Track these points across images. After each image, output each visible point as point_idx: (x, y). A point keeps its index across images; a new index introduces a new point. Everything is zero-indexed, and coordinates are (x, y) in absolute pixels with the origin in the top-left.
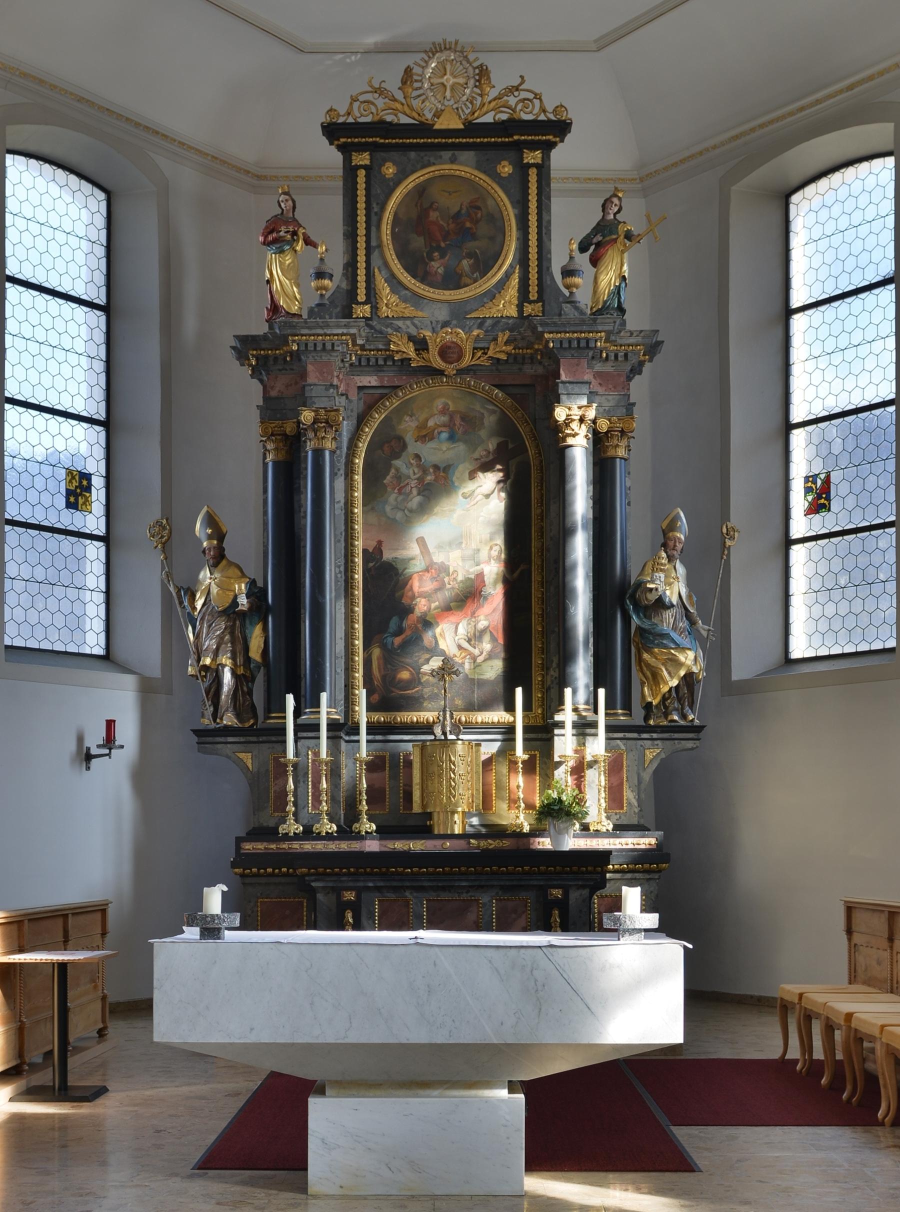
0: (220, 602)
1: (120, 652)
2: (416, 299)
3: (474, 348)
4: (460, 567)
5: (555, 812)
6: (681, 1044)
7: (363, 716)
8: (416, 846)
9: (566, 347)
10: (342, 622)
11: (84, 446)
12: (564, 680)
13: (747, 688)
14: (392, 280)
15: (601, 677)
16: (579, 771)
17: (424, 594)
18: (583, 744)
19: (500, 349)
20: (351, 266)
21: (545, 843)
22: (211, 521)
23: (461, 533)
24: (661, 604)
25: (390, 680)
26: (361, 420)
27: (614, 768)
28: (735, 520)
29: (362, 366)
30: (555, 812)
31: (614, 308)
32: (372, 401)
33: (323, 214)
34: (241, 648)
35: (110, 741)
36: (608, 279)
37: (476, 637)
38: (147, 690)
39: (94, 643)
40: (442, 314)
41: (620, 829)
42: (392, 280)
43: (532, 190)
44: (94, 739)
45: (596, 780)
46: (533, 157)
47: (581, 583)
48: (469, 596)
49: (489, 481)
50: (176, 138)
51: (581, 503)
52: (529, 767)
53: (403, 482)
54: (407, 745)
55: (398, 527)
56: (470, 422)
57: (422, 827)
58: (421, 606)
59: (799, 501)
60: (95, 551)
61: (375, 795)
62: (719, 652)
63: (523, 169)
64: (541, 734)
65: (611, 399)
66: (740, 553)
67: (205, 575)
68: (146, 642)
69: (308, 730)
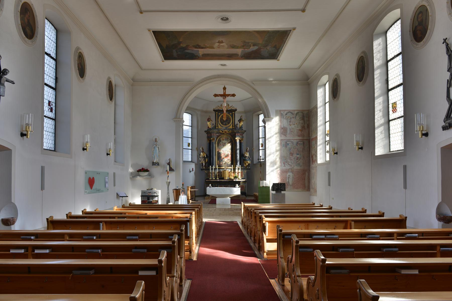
0: (203, 156)
1: (193, 161)
2: (222, 127)
4: (226, 153)
5: (235, 177)
6: (239, 195)
7: (217, 167)
8: (223, 180)
9: (237, 132)
10: (215, 158)
11: (190, 141)
12: (237, 164)
13: (255, 164)
15: (240, 164)
16: (238, 173)
17: (223, 156)
18: (239, 171)
19: (230, 132)
20: (216, 123)
21: (235, 180)
23: (226, 150)
24: (246, 157)
25: (220, 164)
26: (217, 138)
27: (242, 173)
28: (254, 147)
29: (217, 133)
30: (235, 177)
31: (241, 128)
32: (218, 136)
33: (213, 118)
35: (193, 170)
36: (241, 125)
37: (228, 160)
38: (196, 165)
39: (190, 160)
41: (242, 179)
43: (233, 116)
44: (191, 170)
45: (240, 174)
46: (233, 113)
47: (238, 155)
48: (227, 156)
49: (229, 144)
51: (238, 147)
52: (233, 173)
53: (221, 144)
54: (221, 170)
55: (220, 149)
56: (228, 139)
57: (223, 179)
58: (223, 157)
59: (260, 146)
60: (190, 151)
61: (218, 175)
62: (252, 161)
64: (234, 169)
65: (241, 137)
66: (254, 151)
67: (202, 153)
68: (195, 160)
69: (212, 169)
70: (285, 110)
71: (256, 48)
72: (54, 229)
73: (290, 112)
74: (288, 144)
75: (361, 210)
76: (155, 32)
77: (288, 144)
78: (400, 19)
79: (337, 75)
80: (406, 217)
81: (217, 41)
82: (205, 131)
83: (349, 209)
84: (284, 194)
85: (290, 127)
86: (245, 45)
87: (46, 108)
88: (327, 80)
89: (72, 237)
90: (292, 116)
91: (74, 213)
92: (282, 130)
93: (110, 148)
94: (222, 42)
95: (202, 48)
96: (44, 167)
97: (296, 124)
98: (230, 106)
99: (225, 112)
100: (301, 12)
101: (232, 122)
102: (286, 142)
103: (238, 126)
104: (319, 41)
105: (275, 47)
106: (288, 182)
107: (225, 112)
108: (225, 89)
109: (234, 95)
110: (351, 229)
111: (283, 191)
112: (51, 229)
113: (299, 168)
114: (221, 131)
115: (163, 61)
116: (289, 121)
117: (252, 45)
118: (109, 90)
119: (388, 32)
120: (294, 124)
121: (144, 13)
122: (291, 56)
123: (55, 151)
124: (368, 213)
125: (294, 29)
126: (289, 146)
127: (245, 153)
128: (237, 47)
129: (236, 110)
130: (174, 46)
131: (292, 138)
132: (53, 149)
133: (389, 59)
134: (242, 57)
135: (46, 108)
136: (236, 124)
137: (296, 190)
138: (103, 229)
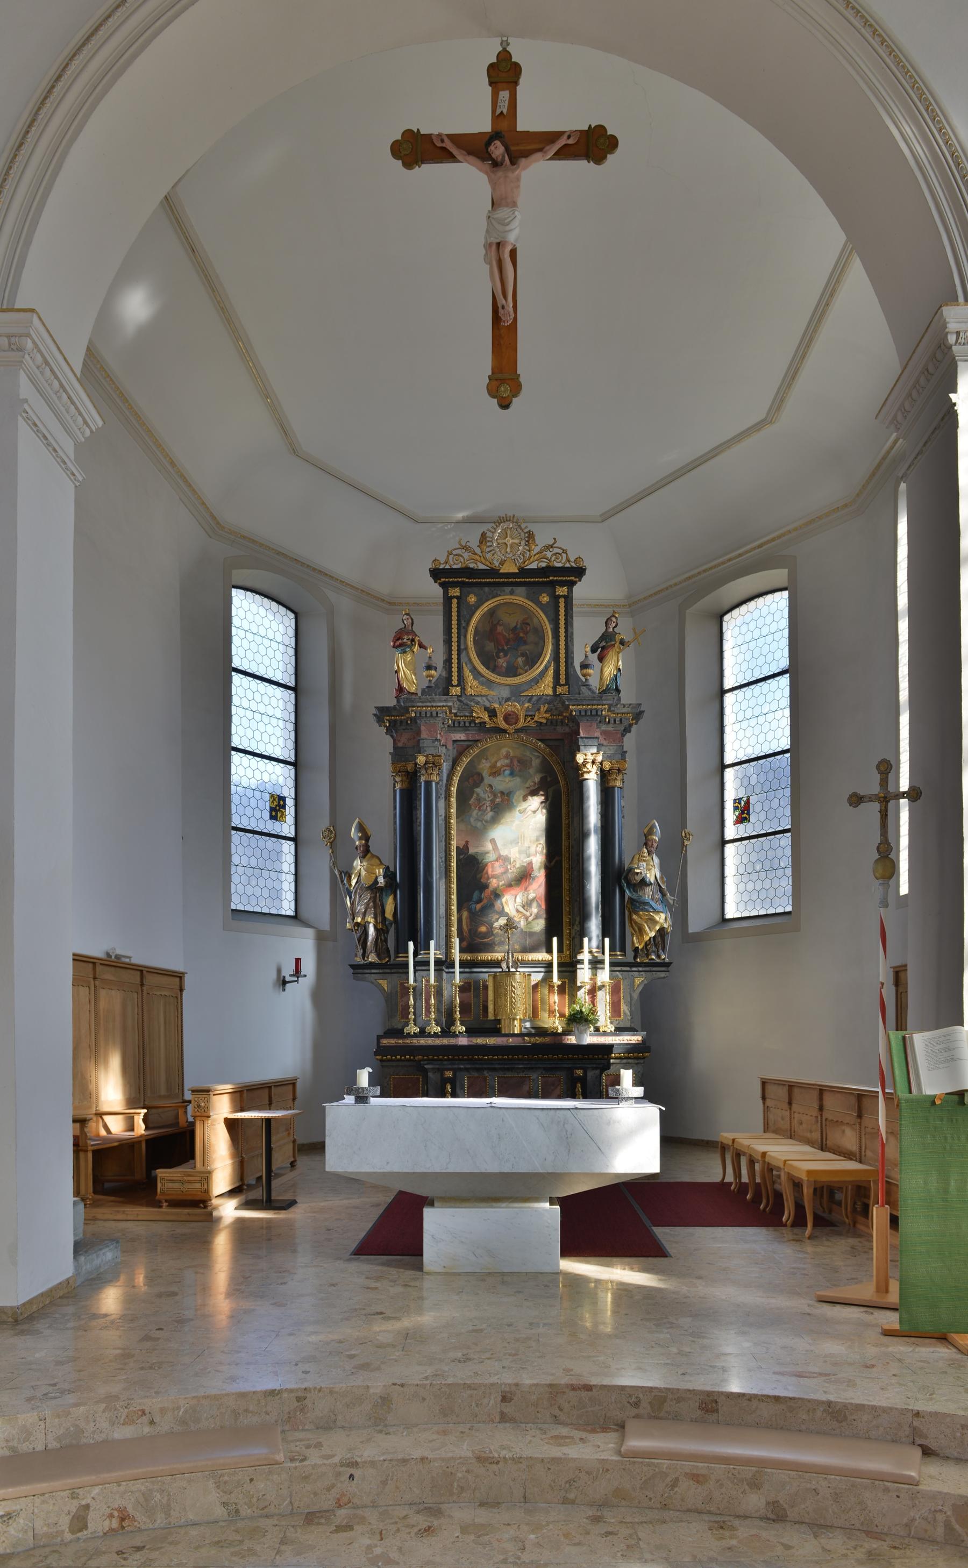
14: (474, 670)
20: (448, 661)
22: (361, 828)
35: (297, 972)
42: (474, 670)
43: (561, 613)
44: (288, 971)
63: (556, 598)
108: (504, 73)
136: (577, 660)
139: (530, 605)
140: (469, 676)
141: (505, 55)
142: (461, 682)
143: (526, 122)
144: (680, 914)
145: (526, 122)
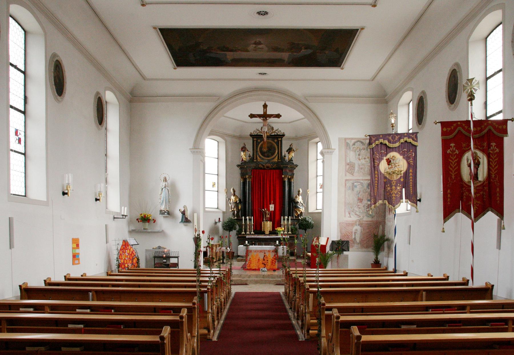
3: (346, 180)
14: (259, 156)
20: (253, 154)
22: (233, 190)
33: (249, 147)
34: (237, 207)
35: (219, 221)
40: (267, 161)
42: (259, 156)
43: (280, 144)
44: (217, 220)
46: (280, 139)
50: (363, 177)
59: (319, 187)
63: (278, 141)
70: (352, 139)
71: (309, 51)
72: (29, 298)
73: (360, 141)
74: (356, 186)
75: (442, 277)
76: (160, 29)
77: (356, 186)
78: (501, 23)
79: (423, 92)
80: (493, 286)
81: (253, 42)
82: (238, 166)
83: (428, 275)
84: (347, 255)
85: (360, 162)
86: (294, 47)
87: (13, 138)
88: (410, 98)
89: (54, 308)
90: (362, 147)
91: (54, 280)
92: (348, 166)
93: (100, 191)
94: (260, 43)
95: (231, 51)
96: (12, 218)
97: (368, 158)
98: (275, 129)
99: (265, 139)
100: (370, 7)
101: (278, 152)
102: (353, 184)
103: (287, 159)
104: (395, 50)
105: (337, 50)
106: (355, 239)
107: (265, 139)
108: (265, 106)
109: (278, 116)
110: (422, 300)
111: (346, 251)
112: (25, 299)
113: (370, 219)
114: (260, 166)
115: (175, 69)
116: (358, 153)
117: (303, 47)
118: (98, 110)
119: (488, 39)
120: (365, 158)
121: (147, 6)
122: (361, 62)
123: (25, 196)
124: (450, 281)
125: (362, 29)
126: (357, 189)
127: (296, 197)
128: (282, 51)
129: (284, 135)
130: (191, 47)
131: (361, 178)
132: (24, 194)
133: (488, 76)
134: (289, 63)
135: (13, 138)
136: (283, 155)
137: (366, 250)
138: (93, 300)
139: (273, 142)
140: (258, 158)
141: (265, 104)
142: (256, 159)
143: (268, 113)
144: (307, 208)
145: (268, 113)
